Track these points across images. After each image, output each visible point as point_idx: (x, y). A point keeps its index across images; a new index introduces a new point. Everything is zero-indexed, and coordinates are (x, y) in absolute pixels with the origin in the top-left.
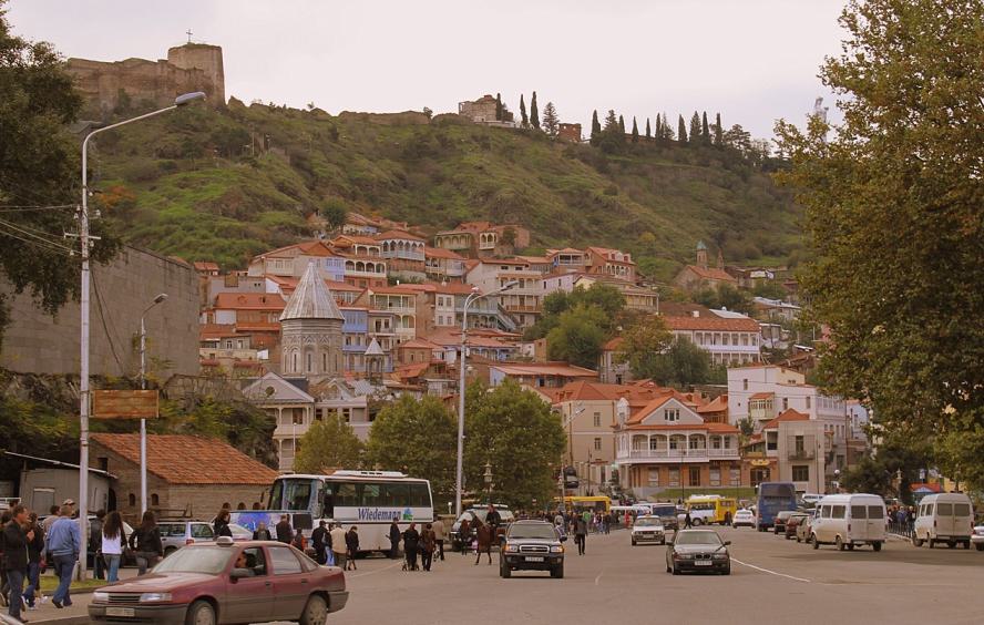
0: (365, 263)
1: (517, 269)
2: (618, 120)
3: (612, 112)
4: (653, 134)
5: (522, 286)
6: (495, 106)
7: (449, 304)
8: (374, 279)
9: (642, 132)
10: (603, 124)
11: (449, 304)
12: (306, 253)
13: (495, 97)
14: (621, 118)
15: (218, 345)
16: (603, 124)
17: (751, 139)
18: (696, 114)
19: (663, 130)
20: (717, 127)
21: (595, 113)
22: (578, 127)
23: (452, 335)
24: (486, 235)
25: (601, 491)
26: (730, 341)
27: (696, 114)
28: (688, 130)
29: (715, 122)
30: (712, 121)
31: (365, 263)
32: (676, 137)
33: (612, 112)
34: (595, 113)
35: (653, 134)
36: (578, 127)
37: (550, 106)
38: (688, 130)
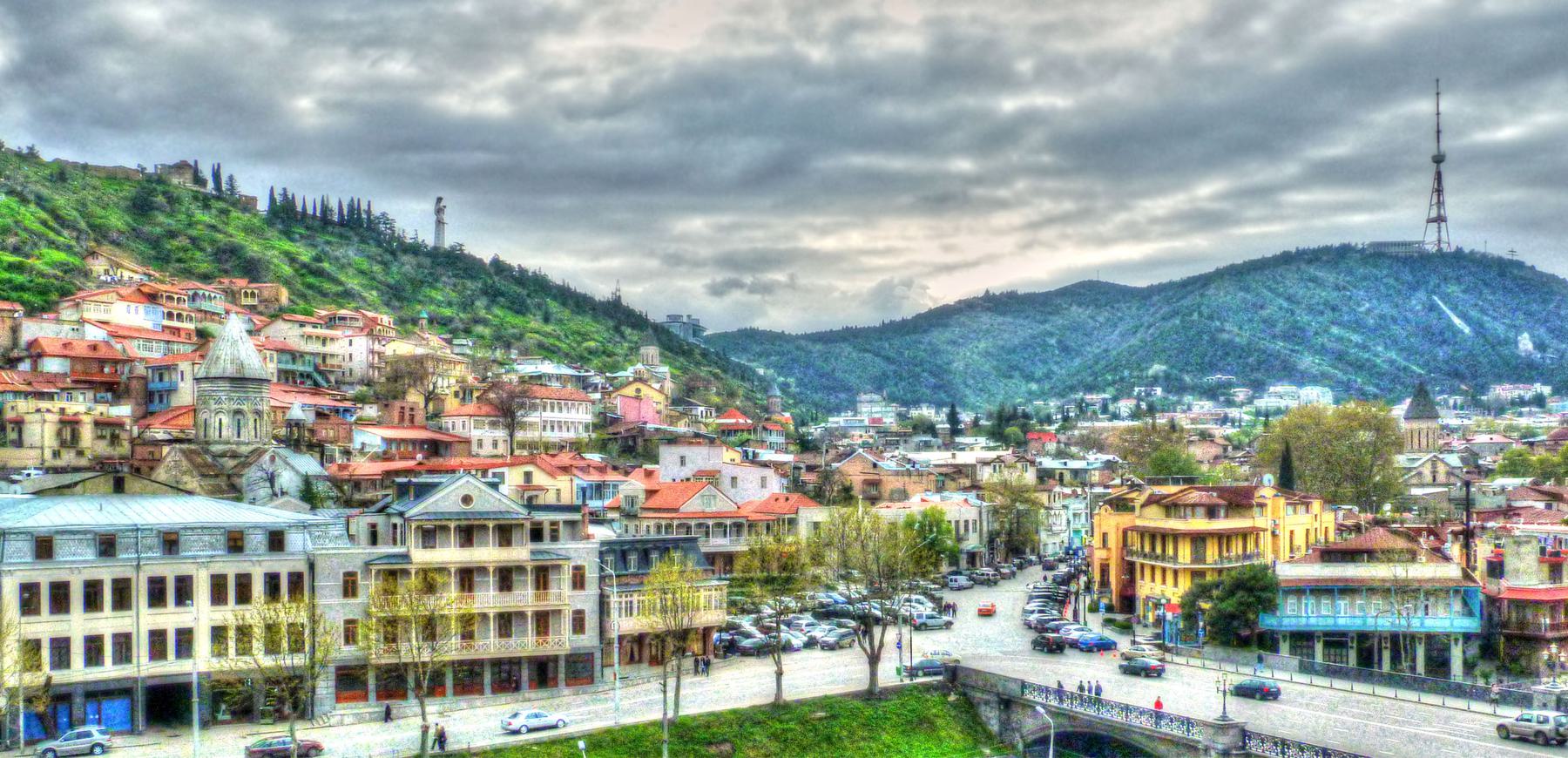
0: (175, 312)
1: (314, 327)
2: (290, 197)
3: (285, 189)
4: (318, 214)
5: (324, 344)
6: (192, 171)
7: (272, 361)
8: (185, 329)
9: (310, 211)
10: (278, 198)
11: (272, 361)
12: (122, 298)
13: (192, 164)
14: (359, 200)
15: (56, 397)
16: (278, 198)
17: (396, 225)
18: (352, 200)
19: (325, 209)
20: (369, 212)
21: (272, 188)
22: (254, 199)
23: (286, 392)
24: (249, 291)
25: (1125, 532)
26: (556, 409)
27: (352, 200)
28: (345, 212)
29: (366, 208)
30: (364, 207)
31: (175, 312)
32: (336, 218)
33: (285, 189)
34: (272, 188)
35: (318, 214)
36: (254, 199)
37: (231, 178)
38: (345, 212)
